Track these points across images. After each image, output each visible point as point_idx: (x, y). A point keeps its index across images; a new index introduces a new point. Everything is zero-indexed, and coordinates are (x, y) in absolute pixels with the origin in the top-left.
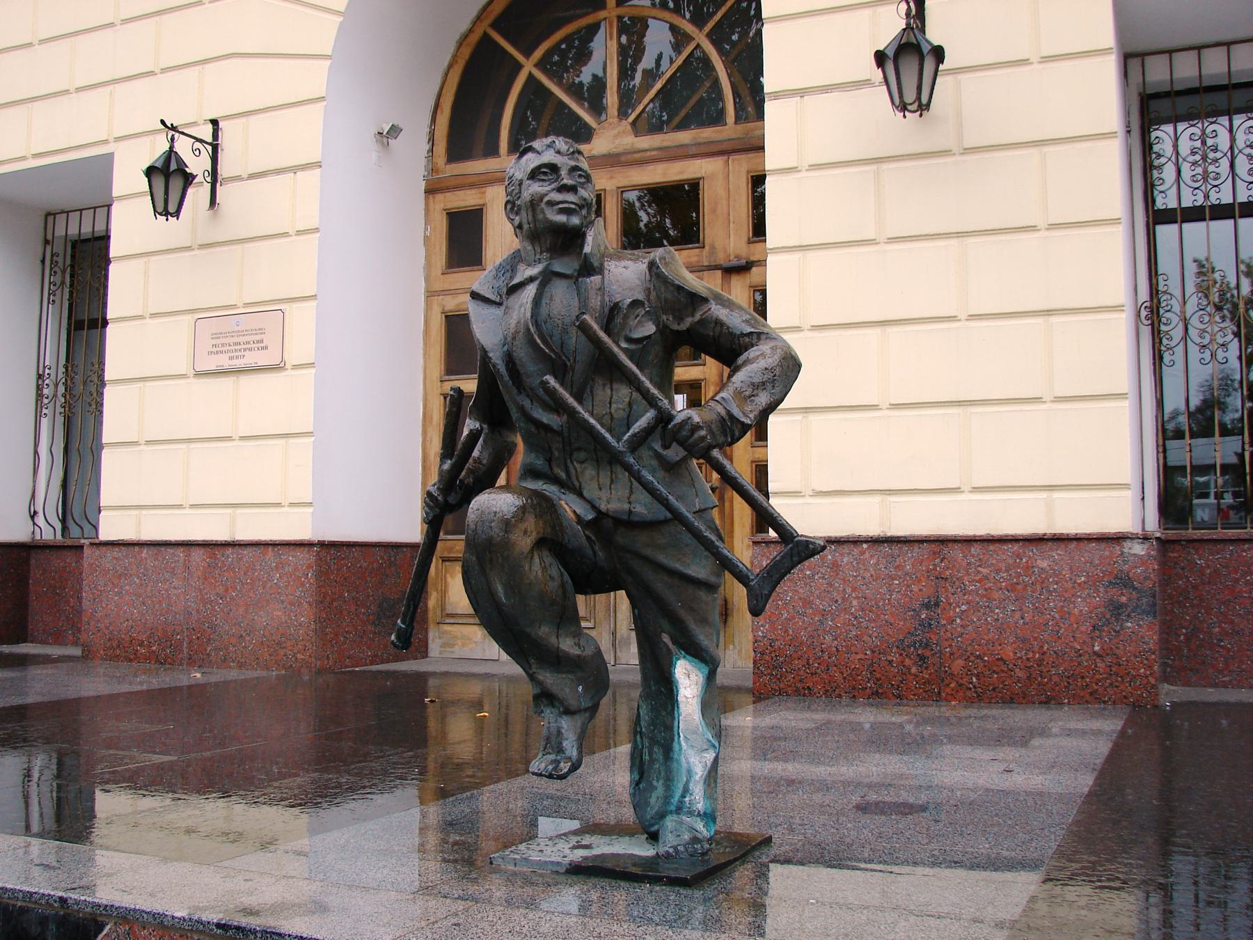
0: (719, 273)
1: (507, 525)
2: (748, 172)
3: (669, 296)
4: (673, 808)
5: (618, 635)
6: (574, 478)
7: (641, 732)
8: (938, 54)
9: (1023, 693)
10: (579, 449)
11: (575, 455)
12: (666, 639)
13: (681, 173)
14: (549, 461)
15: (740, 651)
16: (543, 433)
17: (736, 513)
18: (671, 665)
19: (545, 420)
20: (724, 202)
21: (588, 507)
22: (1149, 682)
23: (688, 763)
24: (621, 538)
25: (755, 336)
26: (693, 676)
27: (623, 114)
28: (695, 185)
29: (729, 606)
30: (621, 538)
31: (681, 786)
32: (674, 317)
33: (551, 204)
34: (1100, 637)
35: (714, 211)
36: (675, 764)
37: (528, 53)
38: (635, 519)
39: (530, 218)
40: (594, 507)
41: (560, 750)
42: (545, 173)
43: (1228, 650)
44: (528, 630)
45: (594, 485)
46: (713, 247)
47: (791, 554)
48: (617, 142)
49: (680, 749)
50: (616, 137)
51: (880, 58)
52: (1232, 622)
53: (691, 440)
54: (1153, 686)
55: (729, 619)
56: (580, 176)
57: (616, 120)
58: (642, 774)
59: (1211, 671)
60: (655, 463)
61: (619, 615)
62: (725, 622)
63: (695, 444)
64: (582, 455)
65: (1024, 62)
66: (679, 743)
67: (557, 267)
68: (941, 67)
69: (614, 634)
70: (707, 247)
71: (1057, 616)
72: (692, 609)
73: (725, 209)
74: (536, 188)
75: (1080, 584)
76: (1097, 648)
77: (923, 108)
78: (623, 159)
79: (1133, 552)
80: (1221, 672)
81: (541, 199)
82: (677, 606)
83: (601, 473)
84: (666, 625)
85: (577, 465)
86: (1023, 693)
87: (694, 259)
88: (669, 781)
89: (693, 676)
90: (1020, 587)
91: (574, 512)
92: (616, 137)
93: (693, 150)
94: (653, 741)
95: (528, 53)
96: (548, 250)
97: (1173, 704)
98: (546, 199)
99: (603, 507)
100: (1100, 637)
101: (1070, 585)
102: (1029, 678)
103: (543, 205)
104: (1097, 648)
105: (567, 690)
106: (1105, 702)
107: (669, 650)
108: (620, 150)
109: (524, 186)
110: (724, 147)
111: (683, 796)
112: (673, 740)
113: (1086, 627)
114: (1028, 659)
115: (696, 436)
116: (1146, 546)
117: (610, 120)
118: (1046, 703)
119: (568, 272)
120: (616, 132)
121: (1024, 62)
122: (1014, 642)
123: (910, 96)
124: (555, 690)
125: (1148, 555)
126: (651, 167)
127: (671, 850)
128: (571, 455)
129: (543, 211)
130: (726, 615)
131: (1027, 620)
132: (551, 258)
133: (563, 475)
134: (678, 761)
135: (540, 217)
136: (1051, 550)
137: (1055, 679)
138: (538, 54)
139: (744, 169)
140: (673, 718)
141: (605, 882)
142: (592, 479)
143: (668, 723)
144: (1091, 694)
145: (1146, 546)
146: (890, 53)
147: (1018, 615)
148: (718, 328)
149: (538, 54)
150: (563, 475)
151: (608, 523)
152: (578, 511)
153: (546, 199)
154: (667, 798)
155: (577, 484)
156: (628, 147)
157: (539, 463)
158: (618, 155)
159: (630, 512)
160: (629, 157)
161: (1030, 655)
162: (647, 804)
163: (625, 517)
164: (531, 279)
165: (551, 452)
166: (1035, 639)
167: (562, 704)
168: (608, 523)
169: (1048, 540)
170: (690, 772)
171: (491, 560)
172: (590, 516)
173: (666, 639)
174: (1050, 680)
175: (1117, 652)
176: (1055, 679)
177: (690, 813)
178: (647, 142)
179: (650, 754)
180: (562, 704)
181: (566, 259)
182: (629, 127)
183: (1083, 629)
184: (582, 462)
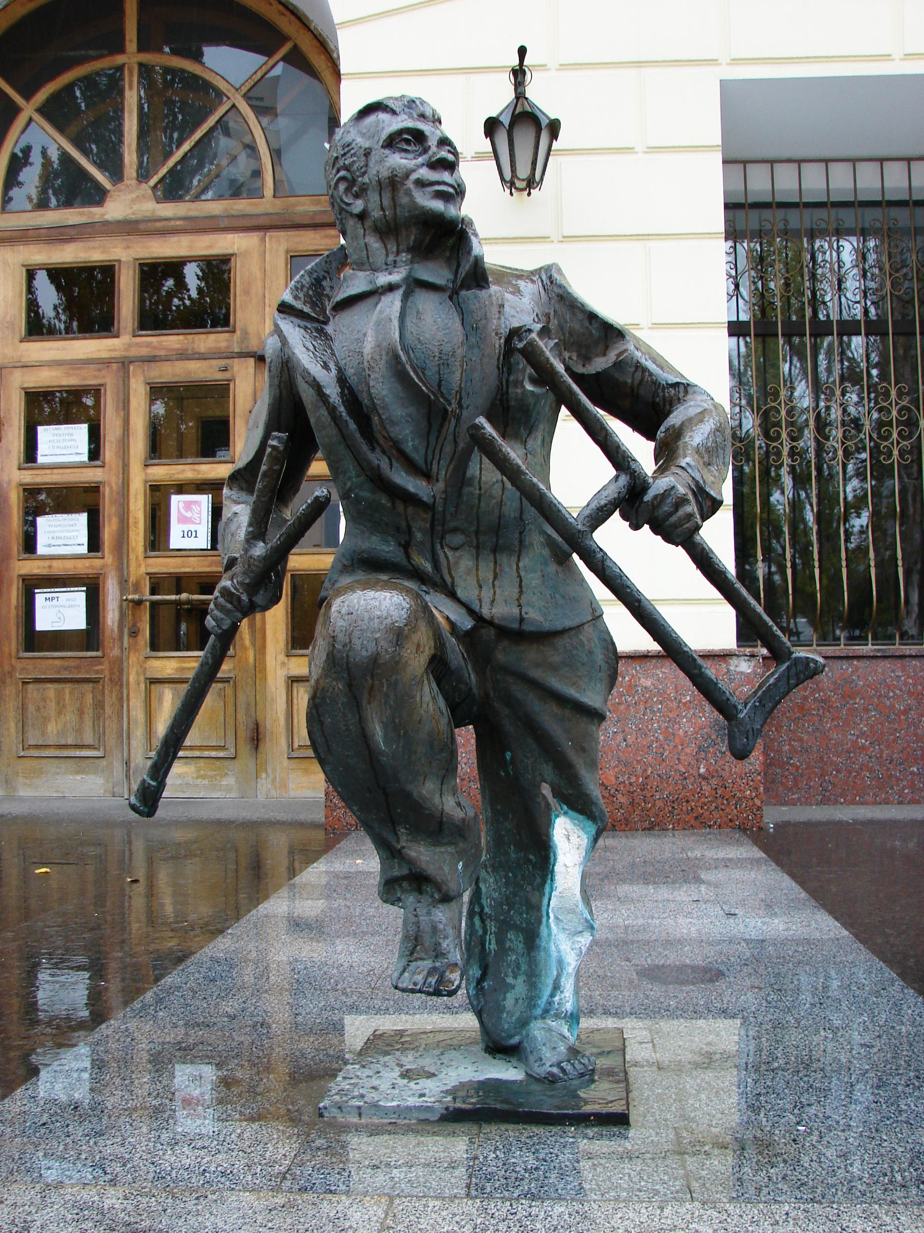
0: (252, 360)
1: (399, 635)
2: (287, 252)
3: (577, 327)
4: (539, 1011)
5: (132, 765)
6: (445, 571)
7: (481, 913)
8: (554, 128)
9: (626, 820)
10: (455, 530)
11: (448, 537)
12: (546, 790)
13: (209, 247)
14: (406, 547)
15: (274, 781)
16: (400, 507)
17: (268, 627)
18: (549, 824)
19: (411, 488)
20: (259, 283)
21: (463, 611)
22: (754, 804)
23: (559, 951)
24: (504, 655)
25: (682, 389)
26: (574, 838)
27: (143, 175)
28: (225, 260)
29: (261, 729)
30: (504, 655)
31: (550, 982)
32: (579, 356)
33: (421, 184)
34: (706, 759)
35: (247, 292)
36: (542, 954)
37: (28, 97)
38: (527, 627)
39: (386, 202)
40: (471, 612)
41: (438, 954)
42: (407, 142)
43: (797, 768)
44: (409, 787)
45: (472, 581)
46: (245, 333)
47: (787, 675)
48: (135, 207)
49: (550, 935)
50: (134, 201)
51: (491, 126)
52: (800, 740)
53: (673, 519)
54: (759, 809)
55: (260, 743)
56: (449, 151)
57: (134, 182)
58: (485, 969)
59: (781, 789)
60: (546, 552)
61: (133, 742)
62: (257, 748)
63: (676, 526)
64: (458, 539)
65: (629, 150)
66: (548, 926)
67: (426, 273)
68: (556, 145)
69: (128, 763)
70: (238, 332)
71: (661, 737)
72: (583, 750)
73: (260, 291)
74: (398, 160)
75: (685, 704)
76: (702, 770)
77: (531, 183)
78: (142, 227)
79: (738, 670)
80: (790, 789)
81: (407, 176)
82: (567, 746)
83: (482, 564)
84: (548, 770)
85: (450, 554)
86: (626, 820)
87: (223, 345)
88: (533, 977)
89: (574, 838)
90: (622, 707)
91: (448, 618)
92: (134, 201)
93: (225, 223)
94: (505, 925)
95: (28, 97)
96: (409, 250)
97: (777, 826)
98: (414, 177)
99: (485, 612)
100: (706, 759)
101: (675, 704)
102: (632, 803)
103: (410, 184)
104: (702, 770)
105: (446, 869)
106: (710, 827)
107: (548, 805)
108: (139, 216)
109: (373, 158)
110: (262, 221)
111: (552, 995)
112: (540, 922)
113: (691, 749)
114: (631, 784)
115: (681, 512)
116: (753, 664)
117: (126, 182)
118: (649, 829)
119: (439, 281)
120: (134, 195)
121: (629, 150)
122: (617, 766)
123: (523, 172)
124: (431, 870)
125: (754, 672)
126: (175, 239)
127: (555, 1070)
128: (442, 538)
129: (408, 193)
130: (258, 740)
131: (630, 742)
132: (412, 262)
133: (428, 567)
134: (546, 950)
135: (404, 200)
136: (655, 667)
137: (659, 804)
138: (41, 96)
139: (282, 248)
140: (542, 894)
141: (512, 1131)
142: (468, 573)
143: (534, 900)
144: (696, 818)
145: (753, 664)
146: (506, 120)
147: (620, 737)
148: (639, 374)
149: (41, 96)
150: (428, 567)
151: (489, 634)
152: (453, 617)
153: (414, 177)
154: (531, 1001)
155: (448, 579)
156: (148, 214)
157: (387, 549)
158: (137, 222)
159: (522, 620)
160: (150, 226)
161: (633, 779)
162: (500, 1009)
163: (515, 626)
164: (391, 288)
165: (409, 532)
166: (638, 762)
167: (439, 890)
168: (489, 634)
169: (653, 657)
170: (560, 963)
171: (372, 688)
172: (467, 624)
173: (546, 790)
174: (654, 805)
175: (724, 774)
176: (659, 804)
177: (557, 1016)
178: (168, 210)
179: (500, 942)
180: (439, 890)
181: (430, 265)
182: (150, 192)
183: (688, 750)
184: (456, 549)
